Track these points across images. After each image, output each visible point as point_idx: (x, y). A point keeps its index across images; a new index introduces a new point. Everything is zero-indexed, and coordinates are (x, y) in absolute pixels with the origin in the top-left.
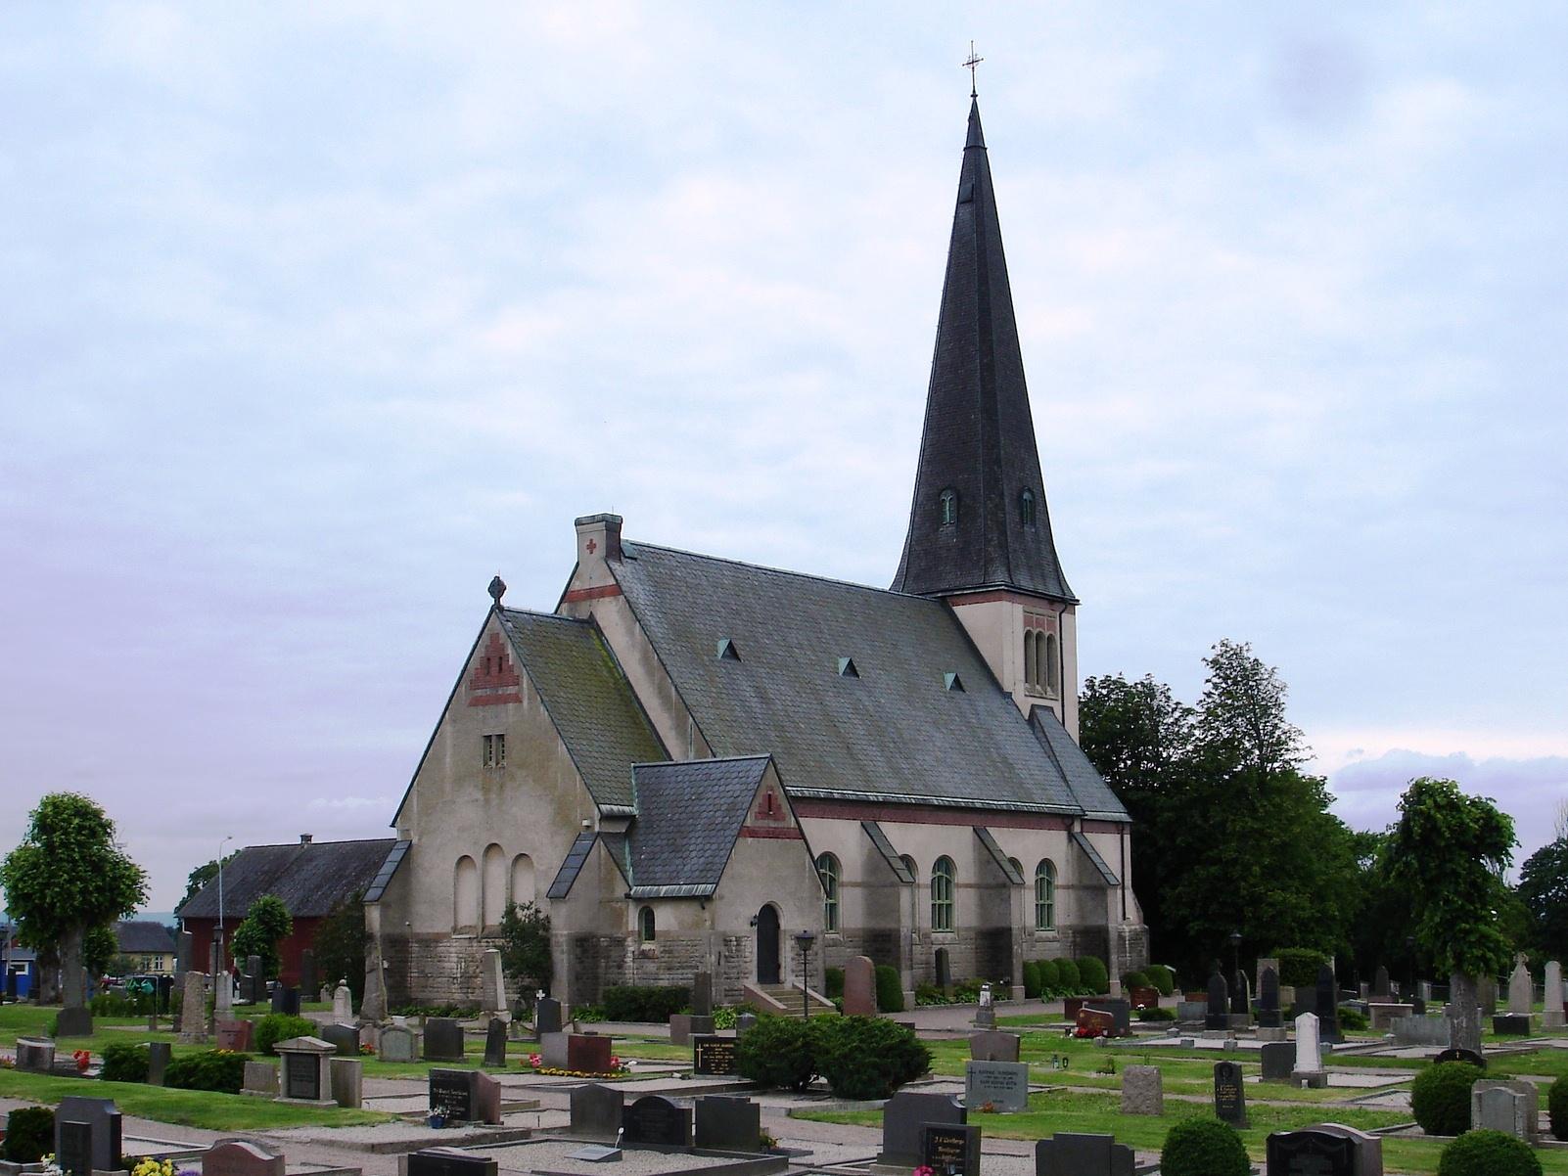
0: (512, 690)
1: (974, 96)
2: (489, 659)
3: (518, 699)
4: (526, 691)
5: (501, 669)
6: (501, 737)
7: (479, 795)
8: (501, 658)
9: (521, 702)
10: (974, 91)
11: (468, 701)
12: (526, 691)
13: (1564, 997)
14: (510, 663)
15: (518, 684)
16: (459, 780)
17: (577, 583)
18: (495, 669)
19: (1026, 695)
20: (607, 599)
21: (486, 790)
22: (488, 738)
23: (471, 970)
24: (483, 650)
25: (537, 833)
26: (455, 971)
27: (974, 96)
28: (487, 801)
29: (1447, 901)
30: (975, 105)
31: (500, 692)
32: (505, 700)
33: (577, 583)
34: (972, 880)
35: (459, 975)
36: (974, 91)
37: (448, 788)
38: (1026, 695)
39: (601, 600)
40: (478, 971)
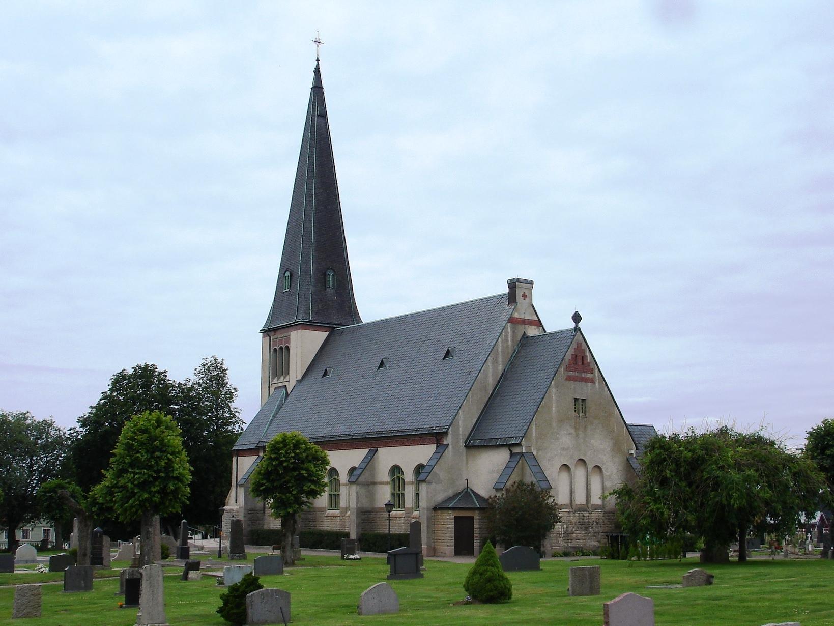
0: (589, 375)
1: (318, 60)
2: (576, 356)
3: (593, 381)
4: (597, 378)
5: (583, 363)
6: (583, 400)
7: (573, 431)
8: (583, 357)
9: (595, 383)
10: (318, 58)
11: (565, 377)
12: (597, 378)
13: (452, 557)
14: (588, 361)
15: (592, 373)
16: (561, 421)
17: (516, 314)
18: (580, 363)
19: (124, 370)
20: (533, 327)
21: (576, 429)
22: (576, 400)
23: (570, 529)
24: (573, 350)
25: (605, 455)
26: (560, 530)
27: (318, 60)
28: (577, 435)
29: (83, 503)
30: (318, 65)
31: (583, 376)
32: (586, 380)
33: (516, 314)
34: (380, 487)
35: (563, 533)
36: (318, 58)
37: (554, 424)
38: (124, 370)
39: (530, 326)
40: (574, 530)
